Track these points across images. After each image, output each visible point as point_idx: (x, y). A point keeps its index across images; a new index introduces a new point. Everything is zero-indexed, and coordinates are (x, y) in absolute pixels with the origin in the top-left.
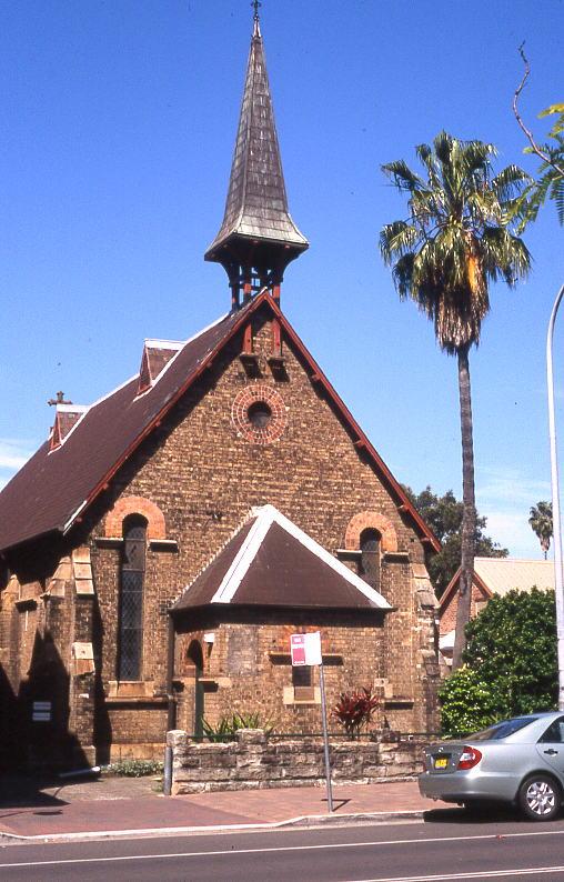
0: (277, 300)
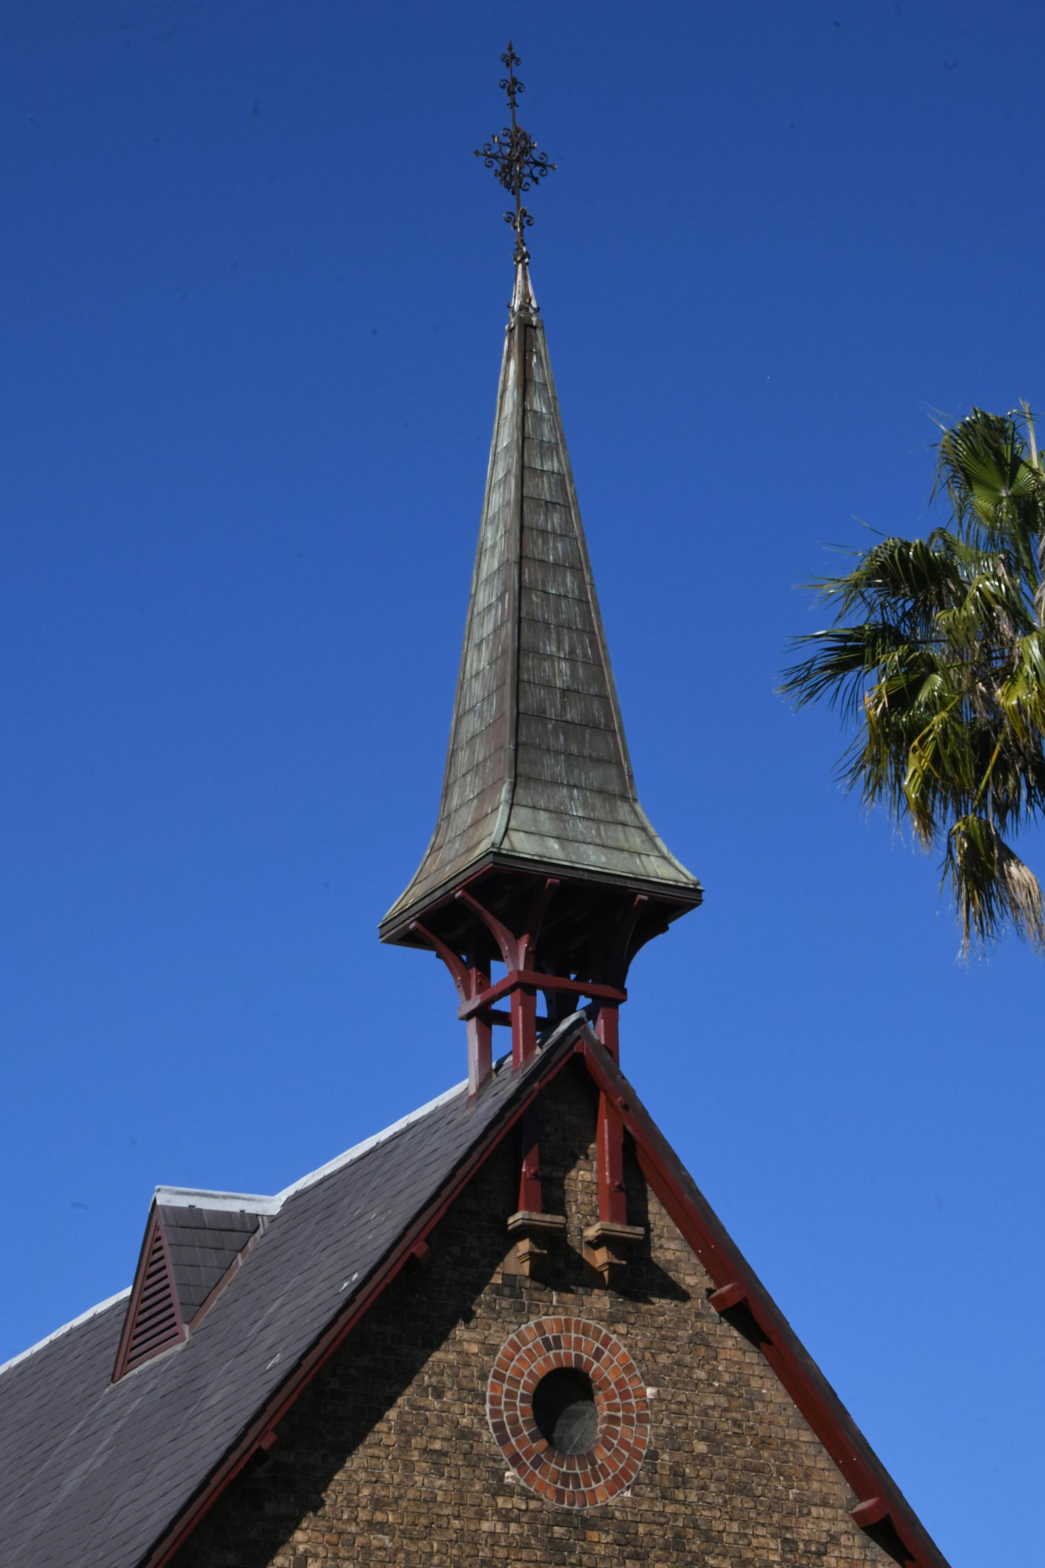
0: (612, 1048)
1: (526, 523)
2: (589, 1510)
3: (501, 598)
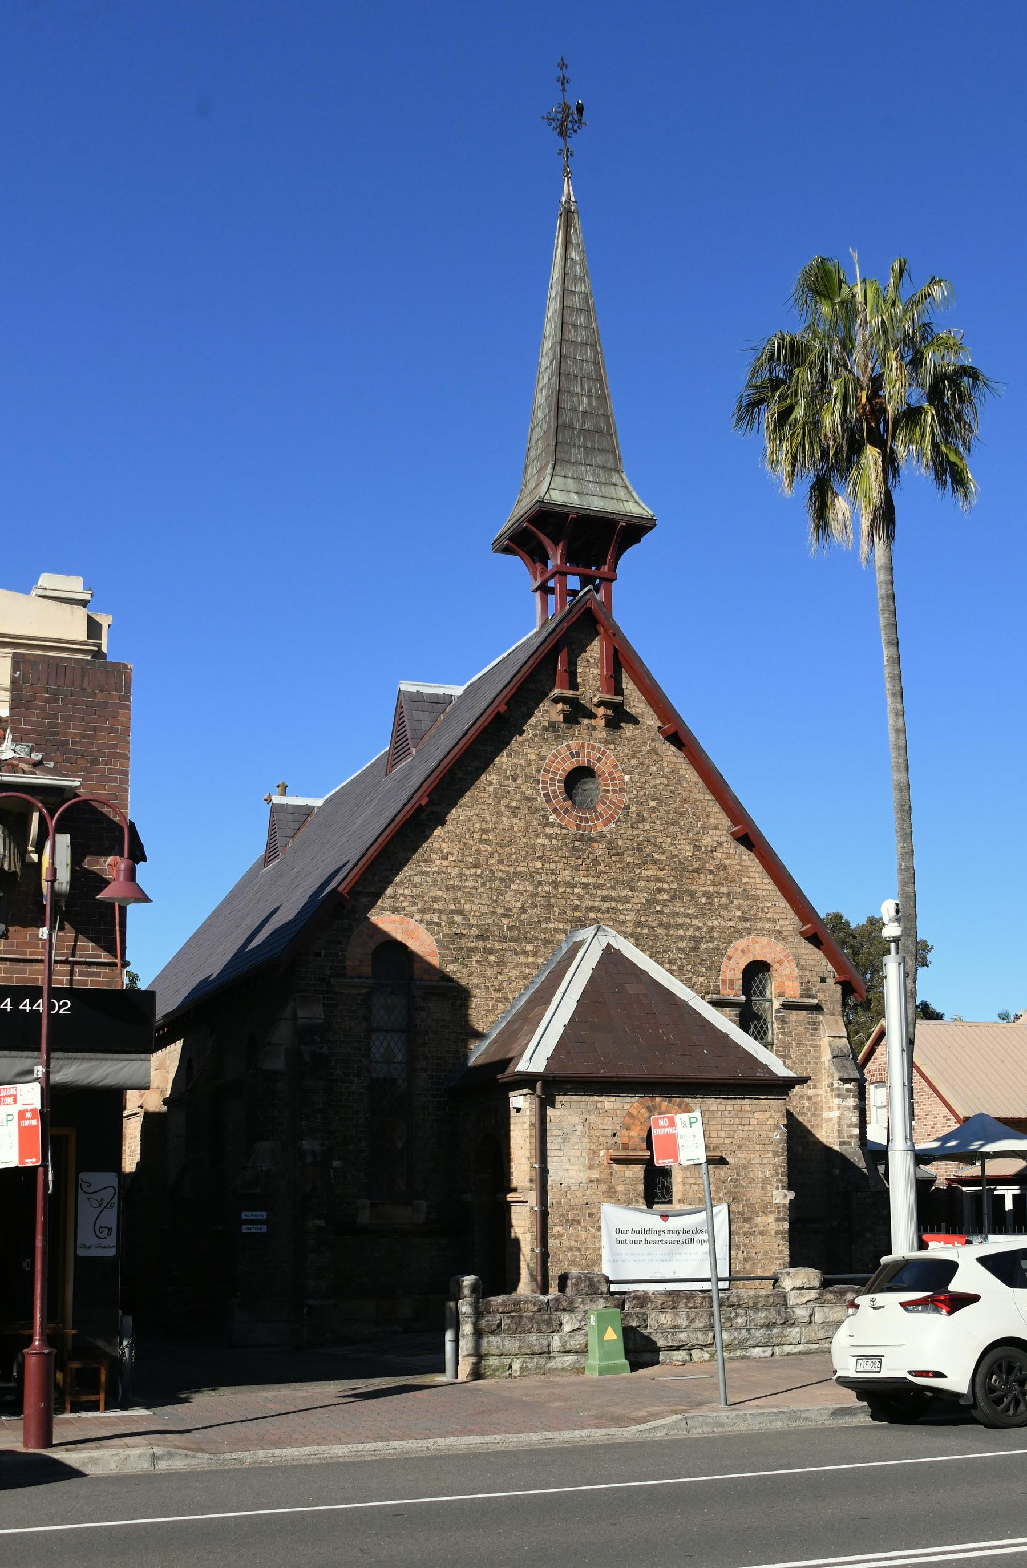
1: (565, 321)
2: (593, 834)
3: (551, 363)
